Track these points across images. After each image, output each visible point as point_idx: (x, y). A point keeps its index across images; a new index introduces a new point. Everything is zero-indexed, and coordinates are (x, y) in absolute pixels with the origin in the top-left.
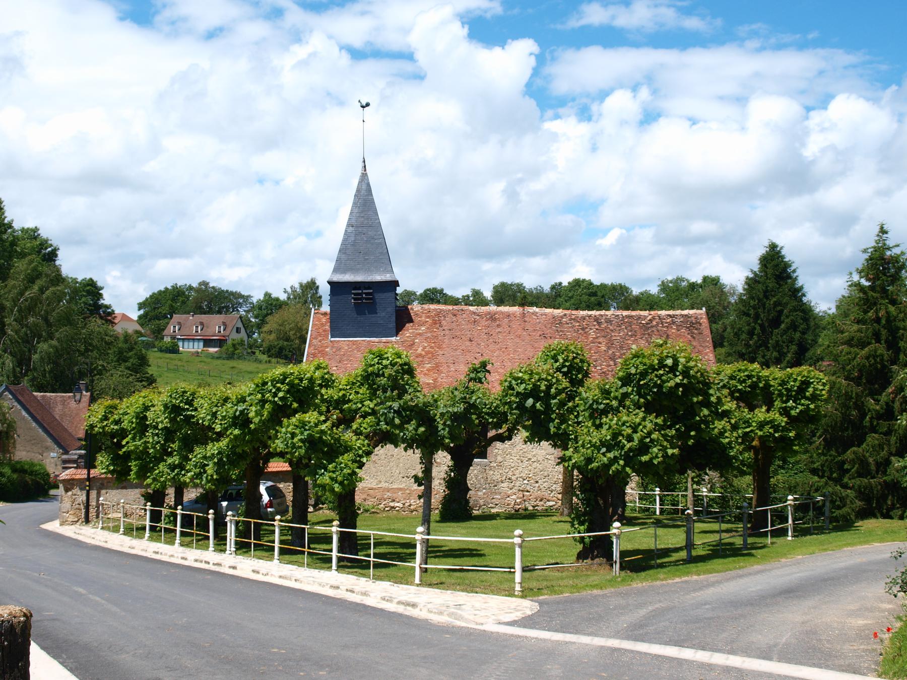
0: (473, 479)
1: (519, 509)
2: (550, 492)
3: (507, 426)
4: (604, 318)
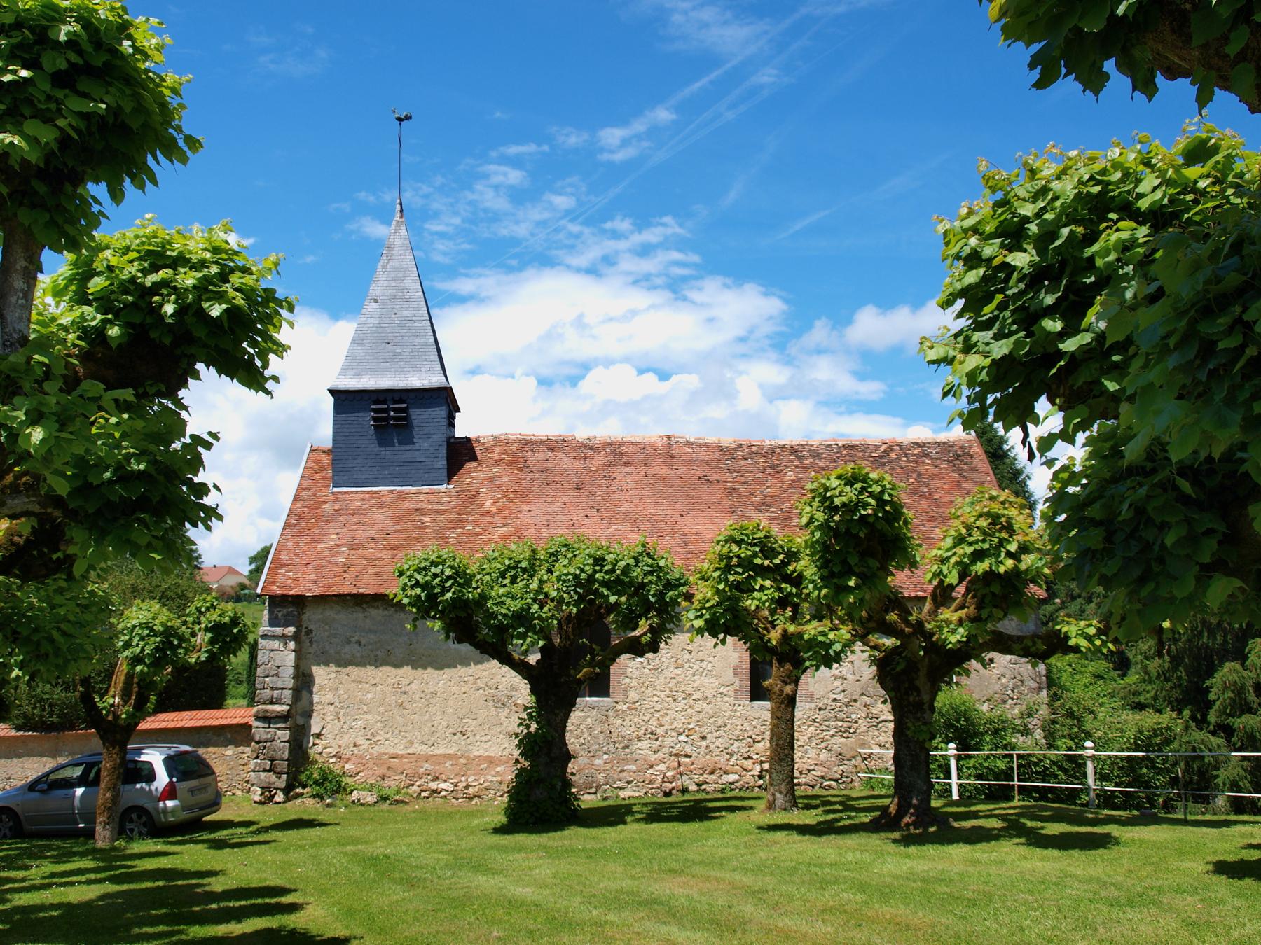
0: (585, 736)
1: (671, 790)
2: (728, 756)
3: (649, 622)
4: (807, 449)
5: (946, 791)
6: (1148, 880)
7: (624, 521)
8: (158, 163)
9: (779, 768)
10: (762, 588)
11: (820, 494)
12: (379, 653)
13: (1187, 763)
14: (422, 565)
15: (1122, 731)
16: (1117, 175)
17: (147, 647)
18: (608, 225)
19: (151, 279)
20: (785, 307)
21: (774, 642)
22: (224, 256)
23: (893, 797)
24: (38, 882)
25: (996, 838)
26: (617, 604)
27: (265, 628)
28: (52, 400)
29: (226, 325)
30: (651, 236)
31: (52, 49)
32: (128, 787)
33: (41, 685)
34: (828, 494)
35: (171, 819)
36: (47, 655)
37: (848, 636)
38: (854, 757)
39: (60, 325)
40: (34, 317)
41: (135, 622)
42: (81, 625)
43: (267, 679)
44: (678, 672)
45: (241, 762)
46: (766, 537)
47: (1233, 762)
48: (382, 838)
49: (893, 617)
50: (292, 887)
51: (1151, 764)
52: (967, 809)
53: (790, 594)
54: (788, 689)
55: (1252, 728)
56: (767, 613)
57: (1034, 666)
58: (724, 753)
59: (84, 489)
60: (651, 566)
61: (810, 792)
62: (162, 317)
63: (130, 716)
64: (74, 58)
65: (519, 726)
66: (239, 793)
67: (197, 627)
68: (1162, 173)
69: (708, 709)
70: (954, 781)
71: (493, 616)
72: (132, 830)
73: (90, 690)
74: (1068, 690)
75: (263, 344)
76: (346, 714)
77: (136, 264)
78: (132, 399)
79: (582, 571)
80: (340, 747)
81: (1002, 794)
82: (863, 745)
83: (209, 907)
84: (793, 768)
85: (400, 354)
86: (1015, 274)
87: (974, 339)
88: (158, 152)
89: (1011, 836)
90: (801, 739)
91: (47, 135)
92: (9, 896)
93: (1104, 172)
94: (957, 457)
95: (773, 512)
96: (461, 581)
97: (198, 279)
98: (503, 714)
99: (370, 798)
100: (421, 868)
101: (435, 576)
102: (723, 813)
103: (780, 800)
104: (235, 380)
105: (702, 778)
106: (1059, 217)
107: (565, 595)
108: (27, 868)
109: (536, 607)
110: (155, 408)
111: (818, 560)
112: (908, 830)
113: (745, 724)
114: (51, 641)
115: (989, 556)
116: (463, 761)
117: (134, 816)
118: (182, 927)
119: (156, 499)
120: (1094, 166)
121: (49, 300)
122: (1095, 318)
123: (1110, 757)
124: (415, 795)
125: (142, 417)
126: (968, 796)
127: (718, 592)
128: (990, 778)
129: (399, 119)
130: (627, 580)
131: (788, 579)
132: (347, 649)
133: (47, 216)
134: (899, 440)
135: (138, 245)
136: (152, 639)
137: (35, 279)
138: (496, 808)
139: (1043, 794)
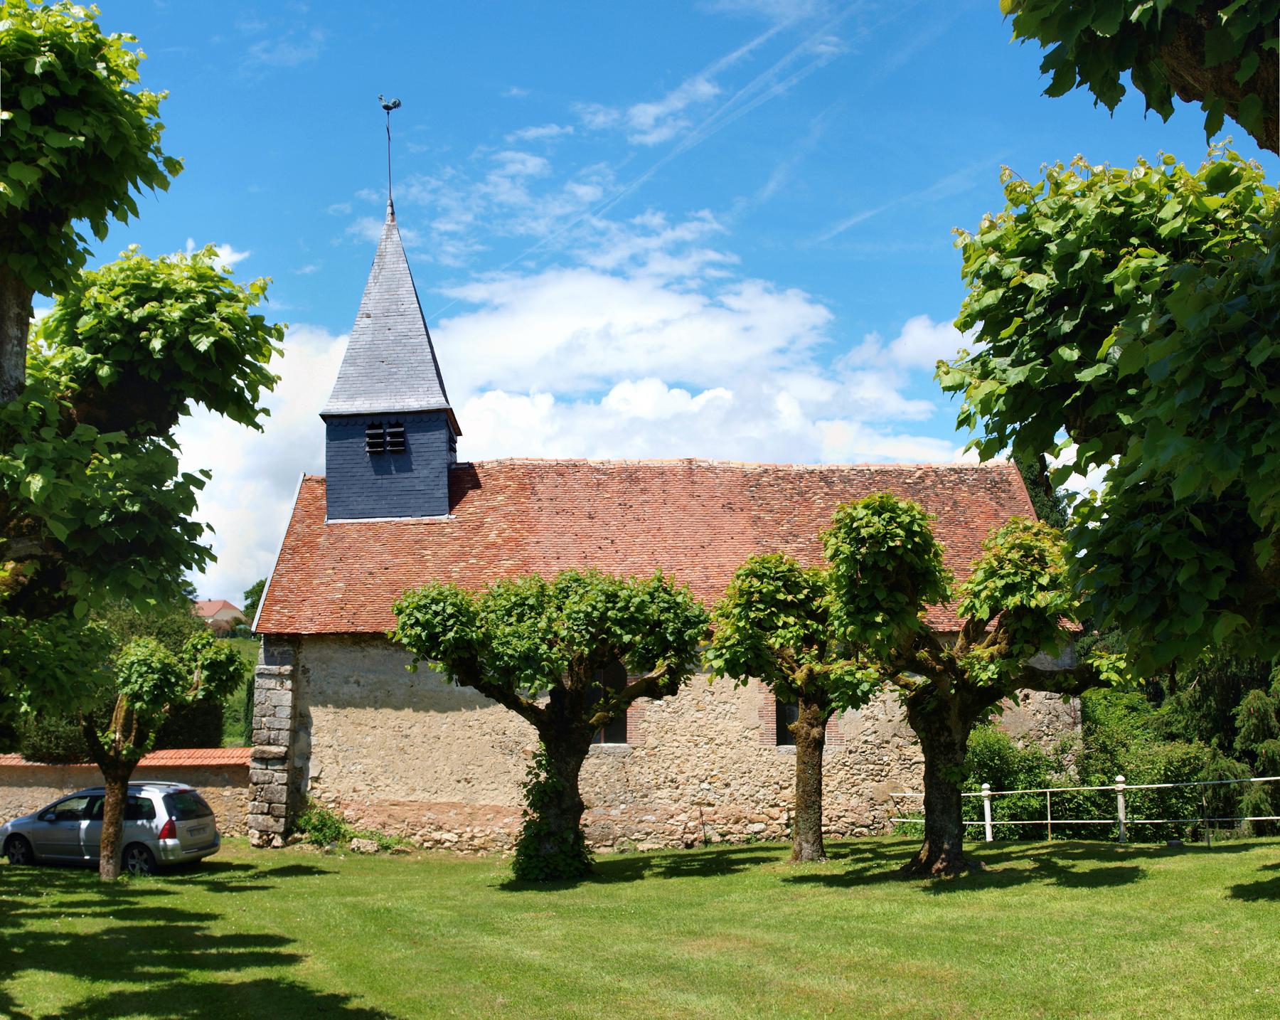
0: (601, 784)
1: (692, 842)
2: (753, 804)
3: (667, 662)
4: (837, 475)
5: (980, 833)
6: (1171, 911)
7: (640, 554)
8: (140, 192)
9: (806, 816)
10: (785, 625)
11: (846, 524)
12: (378, 693)
13: (1214, 789)
14: (422, 603)
15: (1153, 762)
16: (1140, 198)
17: (145, 684)
18: (638, 220)
19: (139, 313)
20: (831, 317)
21: (799, 683)
22: (209, 284)
23: (924, 842)
24: (48, 910)
25: (1028, 879)
26: (631, 645)
27: (261, 667)
28: (49, 447)
29: (214, 358)
30: (685, 232)
31: (29, 84)
32: (129, 823)
33: (47, 718)
34: (855, 525)
35: (171, 858)
36: (52, 692)
37: (876, 675)
38: (886, 802)
39: (53, 367)
40: (29, 361)
41: (134, 658)
42: (84, 664)
43: (264, 719)
44: (699, 715)
45: (240, 803)
46: (789, 570)
47: (1256, 787)
48: (384, 890)
49: (923, 654)
50: (291, 937)
51: (1179, 793)
52: (1000, 851)
53: (816, 631)
54: (815, 732)
55: (1273, 752)
56: (792, 651)
57: (1066, 701)
58: (749, 801)
59: (83, 532)
60: (667, 602)
61: (840, 840)
62: (150, 353)
63: (131, 752)
64: (51, 91)
65: (527, 775)
66: (237, 835)
67: (193, 665)
68: (1183, 199)
69: (731, 753)
70: (988, 822)
71: (499, 657)
72: (134, 866)
73: (94, 724)
74: (1102, 724)
75: (252, 375)
76: (345, 758)
77: (122, 299)
78: (125, 441)
79: (594, 608)
80: (339, 791)
81: (1036, 834)
82: (895, 788)
83: (209, 951)
84: (821, 816)
85: (395, 373)
86: (1033, 297)
87: (992, 365)
88: (138, 180)
89: (1043, 876)
90: (829, 784)
91: (30, 177)
92: (23, 921)
93: (1128, 192)
94: (995, 483)
95: (800, 543)
96: (464, 620)
97: (185, 311)
98: (511, 761)
99: (371, 846)
100: (424, 923)
101: (436, 614)
102: (747, 866)
103: (807, 849)
104: (225, 414)
105: (725, 828)
106: (1079, 238)
107: (576, 635)
108: (38, 895)
109: (544, 647)
110: (147, 445)
111: (844, 595)
112: (939, 876)
113: (772, 770)
114: (56, 678)
115: (1020, 590)
116: (468, 810)
117: (136, 852)
118: (182, 970)
119: (150, 539)
120: (1118, 184)
121: (41, 342)
122: (1111, 348)
123: (1141, 790)
124: (417, 845)
125: (134, 456)
126: (1001, 838)
127: (738, 629)
128: (1024, 817)
129: (387, 108)
130: (642, 617)
131: (812, 615)
132: (346, 689)
133: (35, 261)
134: (934, 466)
135: (124, 280)
136: (150, 676)
137: (28, 324)
138: (504, 864)
139: (1077, 831)
